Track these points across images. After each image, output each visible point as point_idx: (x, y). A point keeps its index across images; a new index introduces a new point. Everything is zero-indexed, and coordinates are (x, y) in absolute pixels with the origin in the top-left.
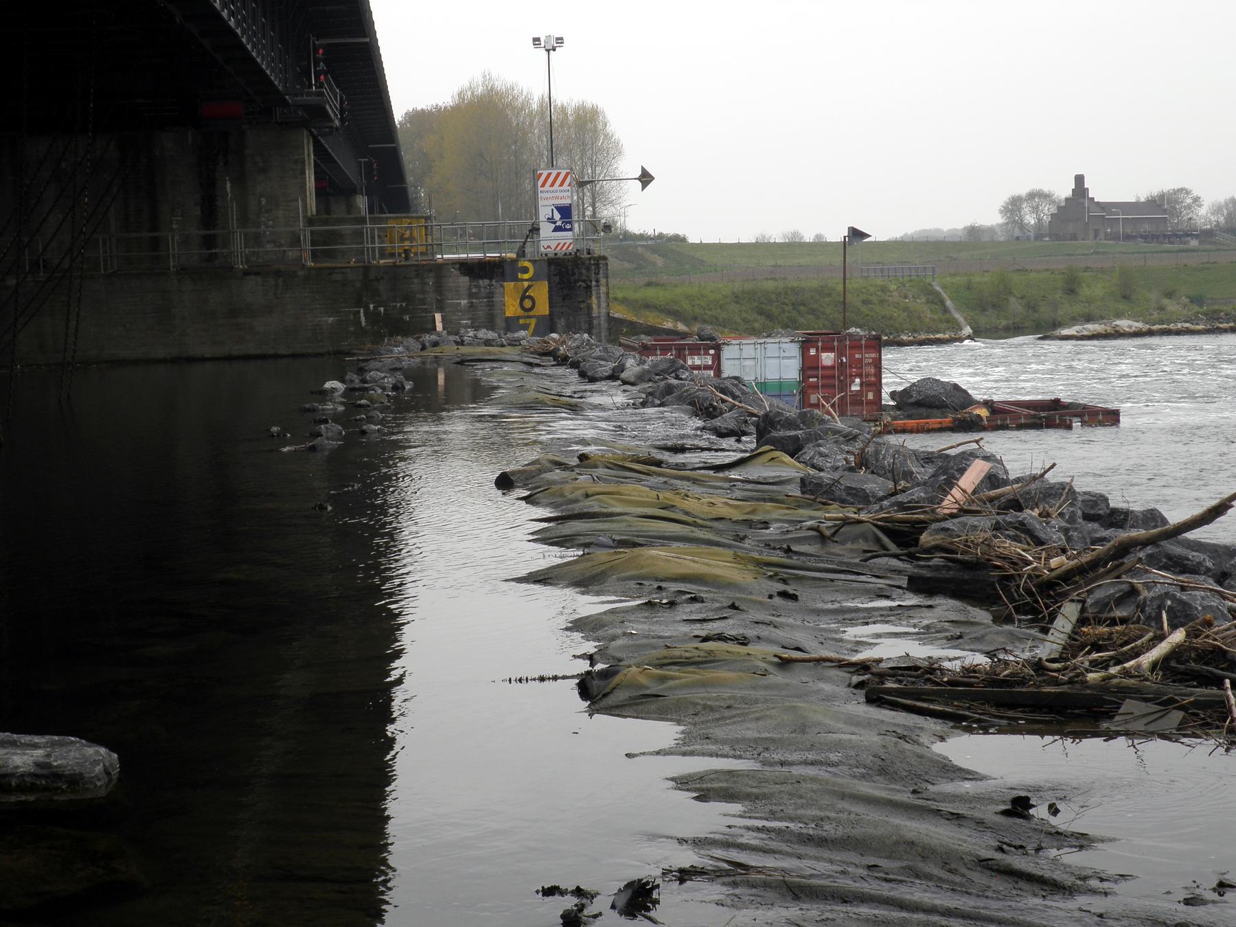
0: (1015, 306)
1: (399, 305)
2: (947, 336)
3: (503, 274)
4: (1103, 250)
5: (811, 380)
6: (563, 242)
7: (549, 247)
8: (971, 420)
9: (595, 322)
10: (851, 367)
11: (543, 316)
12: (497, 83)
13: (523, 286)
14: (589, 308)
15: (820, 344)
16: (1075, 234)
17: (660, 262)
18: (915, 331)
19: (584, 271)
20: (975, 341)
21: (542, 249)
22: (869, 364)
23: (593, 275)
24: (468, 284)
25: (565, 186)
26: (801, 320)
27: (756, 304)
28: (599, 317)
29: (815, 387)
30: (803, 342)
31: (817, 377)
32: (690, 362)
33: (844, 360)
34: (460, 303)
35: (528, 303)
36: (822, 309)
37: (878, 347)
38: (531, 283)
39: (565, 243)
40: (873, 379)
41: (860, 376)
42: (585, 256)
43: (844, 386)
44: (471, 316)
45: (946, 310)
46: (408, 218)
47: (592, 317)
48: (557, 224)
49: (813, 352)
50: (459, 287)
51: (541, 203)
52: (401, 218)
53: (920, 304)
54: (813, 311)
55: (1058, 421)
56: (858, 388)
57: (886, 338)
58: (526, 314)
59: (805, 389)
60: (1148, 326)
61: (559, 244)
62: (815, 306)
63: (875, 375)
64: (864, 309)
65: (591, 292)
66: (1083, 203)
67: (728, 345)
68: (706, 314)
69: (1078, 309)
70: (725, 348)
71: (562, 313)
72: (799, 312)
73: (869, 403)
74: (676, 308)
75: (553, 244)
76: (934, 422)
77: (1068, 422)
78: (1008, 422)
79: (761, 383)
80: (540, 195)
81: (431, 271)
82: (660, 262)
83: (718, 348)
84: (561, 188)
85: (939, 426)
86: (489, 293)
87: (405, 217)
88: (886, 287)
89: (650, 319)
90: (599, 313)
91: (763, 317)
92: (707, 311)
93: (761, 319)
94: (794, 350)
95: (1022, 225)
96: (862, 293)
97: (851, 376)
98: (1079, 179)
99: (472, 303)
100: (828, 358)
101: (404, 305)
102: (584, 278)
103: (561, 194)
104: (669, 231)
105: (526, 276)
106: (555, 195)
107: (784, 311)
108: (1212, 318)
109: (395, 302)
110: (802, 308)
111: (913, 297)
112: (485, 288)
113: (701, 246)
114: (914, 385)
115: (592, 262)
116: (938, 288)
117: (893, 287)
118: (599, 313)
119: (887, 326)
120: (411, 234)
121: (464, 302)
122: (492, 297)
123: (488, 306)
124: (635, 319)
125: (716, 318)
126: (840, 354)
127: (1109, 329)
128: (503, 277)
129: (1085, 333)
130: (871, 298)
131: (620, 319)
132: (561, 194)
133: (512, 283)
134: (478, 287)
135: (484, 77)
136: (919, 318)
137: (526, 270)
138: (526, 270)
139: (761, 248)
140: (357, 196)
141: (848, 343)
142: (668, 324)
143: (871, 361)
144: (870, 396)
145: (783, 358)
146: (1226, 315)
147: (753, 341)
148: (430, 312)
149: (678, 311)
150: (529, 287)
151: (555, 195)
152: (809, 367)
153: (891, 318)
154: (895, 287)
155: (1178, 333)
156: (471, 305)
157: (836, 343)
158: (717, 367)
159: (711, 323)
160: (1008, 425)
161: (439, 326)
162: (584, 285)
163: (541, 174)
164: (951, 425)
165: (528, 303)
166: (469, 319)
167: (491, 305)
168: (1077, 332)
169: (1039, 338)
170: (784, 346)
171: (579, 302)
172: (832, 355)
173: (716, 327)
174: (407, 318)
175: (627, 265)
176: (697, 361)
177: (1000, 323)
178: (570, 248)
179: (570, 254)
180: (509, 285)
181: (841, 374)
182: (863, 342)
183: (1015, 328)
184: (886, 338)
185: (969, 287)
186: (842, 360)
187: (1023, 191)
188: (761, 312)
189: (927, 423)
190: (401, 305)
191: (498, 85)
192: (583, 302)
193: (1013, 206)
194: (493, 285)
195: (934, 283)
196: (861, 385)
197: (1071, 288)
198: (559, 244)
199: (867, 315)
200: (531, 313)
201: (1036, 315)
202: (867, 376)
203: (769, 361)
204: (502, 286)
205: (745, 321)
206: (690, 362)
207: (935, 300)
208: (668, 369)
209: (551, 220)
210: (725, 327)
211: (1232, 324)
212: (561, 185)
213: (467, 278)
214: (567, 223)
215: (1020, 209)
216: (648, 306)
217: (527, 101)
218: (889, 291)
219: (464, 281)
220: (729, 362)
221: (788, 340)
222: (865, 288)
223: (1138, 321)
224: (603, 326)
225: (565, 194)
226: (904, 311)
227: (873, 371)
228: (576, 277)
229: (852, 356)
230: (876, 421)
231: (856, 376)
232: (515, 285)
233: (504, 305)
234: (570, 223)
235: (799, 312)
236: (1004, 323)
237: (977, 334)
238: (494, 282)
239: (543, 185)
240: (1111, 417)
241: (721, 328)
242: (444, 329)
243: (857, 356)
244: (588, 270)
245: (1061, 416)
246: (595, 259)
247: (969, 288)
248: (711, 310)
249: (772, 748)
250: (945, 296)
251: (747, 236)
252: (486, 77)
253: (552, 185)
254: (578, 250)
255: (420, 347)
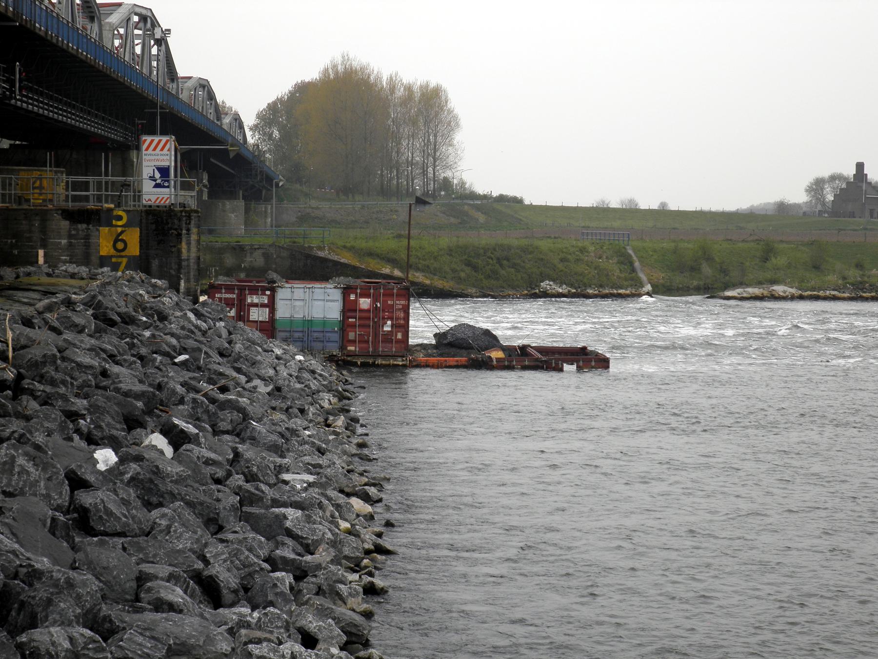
0: (707, 270)
1: (9, 241)
2: (628, 292)
3: (99, 220)
4: (871, 227)
5: (350, 320)
6: (161, 197)
7: (150, 200)
8: (482, 360)
9: (184, 264)
10: (384, 311)
11: (134, 257)
12: (353, 63)
13: (117, 231)
14: (179, 252)
15: (359, 291)
16: (854, 212)
17: (482, 218)
18: (601, 286)
19: (176, 221)
20: (652, 297)
21: (144, 202)
22: (399, 309)
23: (184, 225)
24: (68, 227)
25: (165, 151)
26: (503, 272)
27: (465, 257)
28: (188, 260)
29: (353, 326)
30: (344, 288)
31: (356, 318)
32: (249, 300)
33: (379, 305)
34: (61, 243)
35: (120, 246)
36: (522, 264)
37: (407, 296)
38: (124, 229)
39: (163, 198)
40: (402, 322)
41: (391, 319)
42: (178, 209)
43: (378, 326)
44: (69, 253)
45: (633, 270)
46: (38, 170)
47: (181, 260)
48: (157, 182)
49: (352, 297)
50: (61, 229)
51: (144, 164)
52: (32, 170)
53: (612, 266)
54: (514, 266)
55: (553, 365)
56: (389, 329)
57: (574, 291)
58: (119, 254)
59: (344, 326)
60: (800, 292)
61: (158, 198)
62: (519, 261)
63: (404, 319)
64: (560, 266)
65: (181, 239)
66: (861, 187)
67: (282, 288)
68: (420, 263)
69: (768, 275)
70: (279, 290)
71: (156, 255)
72: (501, 265)
73: (398, 341)
74: (394, 256)
75: (153, 198)
76: (452, 361)
77: (560, 366)
78: (514, 363)
79: (308, 321)
80: (144, 157)
81: (37, 214)
82: (482, 218)
83: (273, 290)
84: (162, 152)
85: (455, 364)
86: (86, 235)
87: (35, 170)
88: (585, 249)
89: (371, 265)
90: (189, 256)
91: (470, 268)
92: (421, 261)
93: (468, 270)
94: (337, 295)
95: (824, 204)
96: (563, 252)
97: (384, 318)
98: (860, 166)
99: (71, 242)
100: (365, 303)
101: (14, 241)
102: (176, 227)
103: (162, 158)
104: (510, 192)
105: (120, 223)
106: (157, 157)
107: (488, 264)
108: (857, 288)
109: (7, 239)
110: (505, 262)
111: (607, 258)
112: (83, 230)
113: (532, 207)
114: (451, 329)
115: (184, 214)
116: (630, 252)
117: (592, 248)
118: (189, 256)
119: (577, 281)
120: (41, 184)
121: (64, 242)
122: (89, 239)
123: (85, 246)
124: (358, 264)
125: (428, 266)
126: (375, 299)
127: (766, 293)
128: (99, 223)
129: (745, 295)
130: (569, 257)
131: (346, 264)
132: (162, 158)
133: (107, 228)
134: (77, 230)
135: (343, 57)
136: (607, 275)
137: (120, 218)
138: (120, 218)
139: (601, 212)
140: (131, 151)
141: (382, 291)
142: (386, 270)
143: (401, 307)
144: (399, 336)
145: (328, 301)
146: (871, 286)
147: (302, 286)
148: (36, 248)
149: (396, 260)
150: (122, 232)
151: (157, 157)
152: (349, 309)
153: (581, 275)
154: (593, 248)
155: (825, 298)
156: (70, 245)
157: (372, 291)
158: (271, 306)
159: (423, 271)
160: (514, 366)
161: (41, 260)
162: (175, 232)
163: (145, 140)
164: (466, 363)
165: (120, 246)
166: (68, 256)
167: (87, 245)
168: (739, 294)
169: (708, 298)
170: (328, 291)
171: (171, 247)
172: (368, 301)
173: (427, 275)
174: (16, 252)
175: (452, 220)
176: (255, 299)
177: (692, 284)
178: (167, 202)
179: (166, 207)
180: (104, 230)
181: (375, 316)
182: (395, 291)
183: (705, 288)
184: (574, 291)
185: (675, 251)
186: (376, 305)
187: (826, 174)
188: (469, 264)
189: (446, 361)
190: (12, 242)
191: (355, 64)
192: (175, 246)
193: (816, 187)
194: (89, 229)
195: (628, 247)
196: (392, 326)
197: (768, 252)
198: (158, 198)
199: (562, 271)
200: (123, 254)
201: (727, 278)
202: (397, 319)
203: (316, 303)
204: (98, 230)
205: (454, 271)
206: (249, 300)
207: (626, 261)
208: (88, 303)
209: (152, 178)
210: (435, 274)
211: (873, 294)
212: (162, 149)
213: (67, 223)
214: (165, 181)
215: (822, 189)
216: (371, 254)
217: (378, 78)
218: (587, 252)
219: (65, 224)
220: (282, 302)
221: (332, 286)
222: (566, 248)
223: (792, 287)
224: (192, 267)
225: (165, 158)
226: (595, 268)
227: (402, 315)
228: (170, 225)
229: (385, 302)
230: (404, 357)
231: (389, 318)
232: (109, 230)
233: (99, 246)
234: (168, 181)
235: (501, 265)
236: (695, 283)
237: (657, 290)
238: (90, 226)
239: (147, 149)
240: (603, 363)
241: (432, 276)
242: (45, 262)
243: (389, 302)
244: (180, 220)
245: (557, 360)
246: (186, 212)
247: (675, 253)
248: (425, 260)
249: (406, 624)
250: (635, 258)
251: (587, 201)
252: (345, 58)
253: (154, 149)
254: (172, 204)
255: (15, 276)
